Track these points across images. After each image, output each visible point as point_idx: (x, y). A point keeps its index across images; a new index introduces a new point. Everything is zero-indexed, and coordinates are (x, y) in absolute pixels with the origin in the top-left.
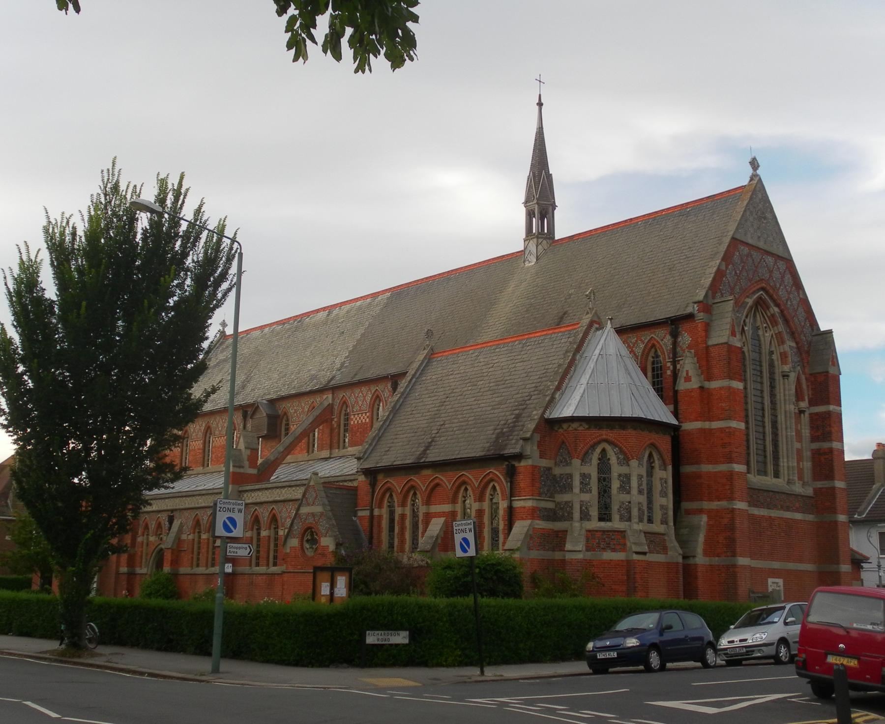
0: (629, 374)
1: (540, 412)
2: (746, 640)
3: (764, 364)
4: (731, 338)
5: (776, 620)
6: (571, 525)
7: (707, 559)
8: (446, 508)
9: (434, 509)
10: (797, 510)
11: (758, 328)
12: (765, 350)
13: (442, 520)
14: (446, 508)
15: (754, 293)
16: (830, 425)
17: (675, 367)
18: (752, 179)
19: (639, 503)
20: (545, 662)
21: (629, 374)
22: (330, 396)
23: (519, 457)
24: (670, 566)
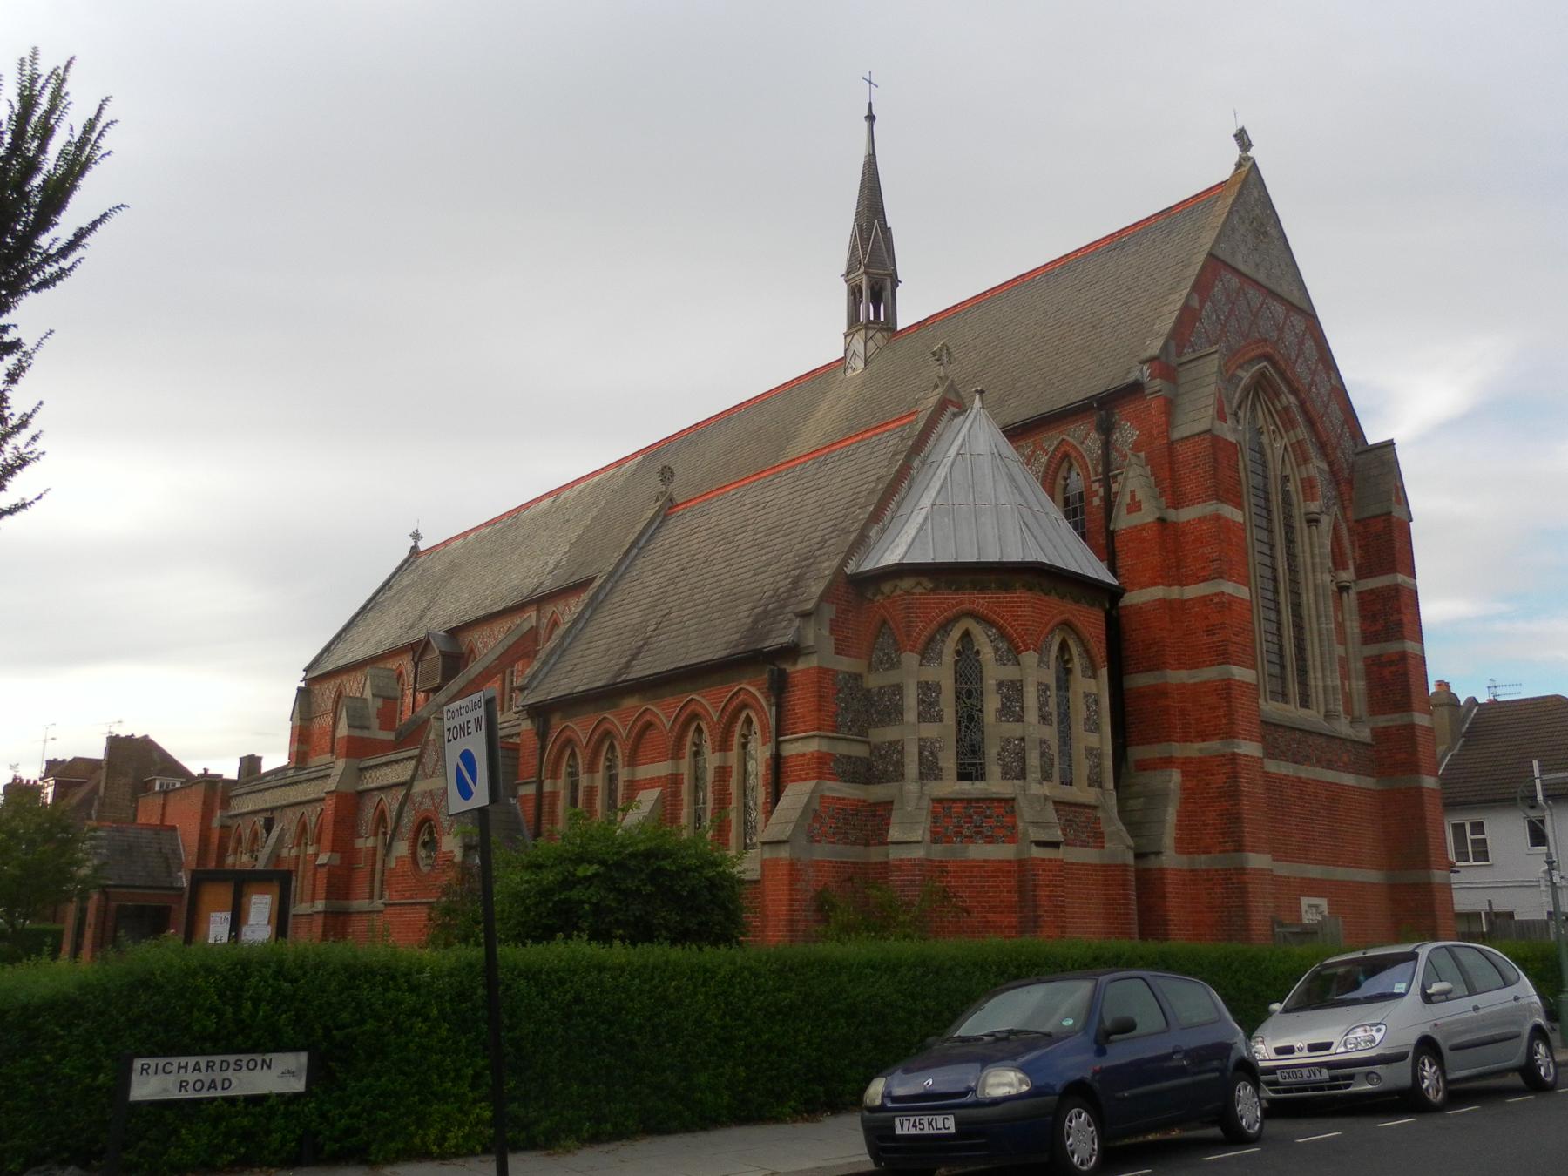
0: (1018, 488)
1: (836, 562)
2: (1327, 1046)
3: (1273, 497)
4: (1217, 423)
5: (1400, 988)
6: (901, 789)
7: (1184, 858)
8: (663, 769)
9: (644, 772)
10: (1345, 768)
11: (1259, 432)
12: (1275, 471)
13: (656, 792)
14: (663, 769)
15: (1251, 362)
16: (1399, 611)
17: (1108, 489)
18: (1239, 165)
19: (1043, 742)
20: (778, 1120)
21: (1018, 488)
22: (534, 614)
23: (792, 651)
24: (1110, 873)
